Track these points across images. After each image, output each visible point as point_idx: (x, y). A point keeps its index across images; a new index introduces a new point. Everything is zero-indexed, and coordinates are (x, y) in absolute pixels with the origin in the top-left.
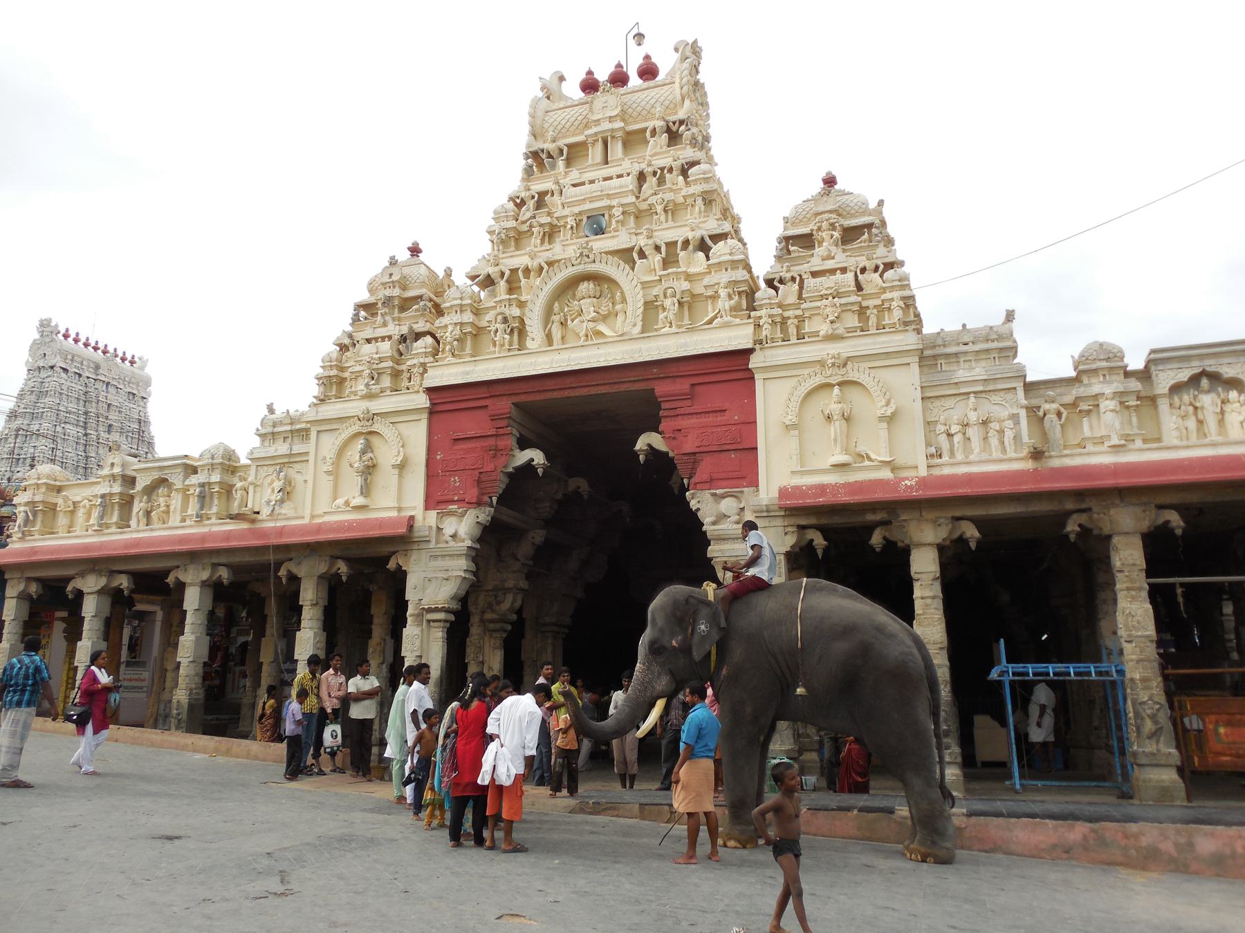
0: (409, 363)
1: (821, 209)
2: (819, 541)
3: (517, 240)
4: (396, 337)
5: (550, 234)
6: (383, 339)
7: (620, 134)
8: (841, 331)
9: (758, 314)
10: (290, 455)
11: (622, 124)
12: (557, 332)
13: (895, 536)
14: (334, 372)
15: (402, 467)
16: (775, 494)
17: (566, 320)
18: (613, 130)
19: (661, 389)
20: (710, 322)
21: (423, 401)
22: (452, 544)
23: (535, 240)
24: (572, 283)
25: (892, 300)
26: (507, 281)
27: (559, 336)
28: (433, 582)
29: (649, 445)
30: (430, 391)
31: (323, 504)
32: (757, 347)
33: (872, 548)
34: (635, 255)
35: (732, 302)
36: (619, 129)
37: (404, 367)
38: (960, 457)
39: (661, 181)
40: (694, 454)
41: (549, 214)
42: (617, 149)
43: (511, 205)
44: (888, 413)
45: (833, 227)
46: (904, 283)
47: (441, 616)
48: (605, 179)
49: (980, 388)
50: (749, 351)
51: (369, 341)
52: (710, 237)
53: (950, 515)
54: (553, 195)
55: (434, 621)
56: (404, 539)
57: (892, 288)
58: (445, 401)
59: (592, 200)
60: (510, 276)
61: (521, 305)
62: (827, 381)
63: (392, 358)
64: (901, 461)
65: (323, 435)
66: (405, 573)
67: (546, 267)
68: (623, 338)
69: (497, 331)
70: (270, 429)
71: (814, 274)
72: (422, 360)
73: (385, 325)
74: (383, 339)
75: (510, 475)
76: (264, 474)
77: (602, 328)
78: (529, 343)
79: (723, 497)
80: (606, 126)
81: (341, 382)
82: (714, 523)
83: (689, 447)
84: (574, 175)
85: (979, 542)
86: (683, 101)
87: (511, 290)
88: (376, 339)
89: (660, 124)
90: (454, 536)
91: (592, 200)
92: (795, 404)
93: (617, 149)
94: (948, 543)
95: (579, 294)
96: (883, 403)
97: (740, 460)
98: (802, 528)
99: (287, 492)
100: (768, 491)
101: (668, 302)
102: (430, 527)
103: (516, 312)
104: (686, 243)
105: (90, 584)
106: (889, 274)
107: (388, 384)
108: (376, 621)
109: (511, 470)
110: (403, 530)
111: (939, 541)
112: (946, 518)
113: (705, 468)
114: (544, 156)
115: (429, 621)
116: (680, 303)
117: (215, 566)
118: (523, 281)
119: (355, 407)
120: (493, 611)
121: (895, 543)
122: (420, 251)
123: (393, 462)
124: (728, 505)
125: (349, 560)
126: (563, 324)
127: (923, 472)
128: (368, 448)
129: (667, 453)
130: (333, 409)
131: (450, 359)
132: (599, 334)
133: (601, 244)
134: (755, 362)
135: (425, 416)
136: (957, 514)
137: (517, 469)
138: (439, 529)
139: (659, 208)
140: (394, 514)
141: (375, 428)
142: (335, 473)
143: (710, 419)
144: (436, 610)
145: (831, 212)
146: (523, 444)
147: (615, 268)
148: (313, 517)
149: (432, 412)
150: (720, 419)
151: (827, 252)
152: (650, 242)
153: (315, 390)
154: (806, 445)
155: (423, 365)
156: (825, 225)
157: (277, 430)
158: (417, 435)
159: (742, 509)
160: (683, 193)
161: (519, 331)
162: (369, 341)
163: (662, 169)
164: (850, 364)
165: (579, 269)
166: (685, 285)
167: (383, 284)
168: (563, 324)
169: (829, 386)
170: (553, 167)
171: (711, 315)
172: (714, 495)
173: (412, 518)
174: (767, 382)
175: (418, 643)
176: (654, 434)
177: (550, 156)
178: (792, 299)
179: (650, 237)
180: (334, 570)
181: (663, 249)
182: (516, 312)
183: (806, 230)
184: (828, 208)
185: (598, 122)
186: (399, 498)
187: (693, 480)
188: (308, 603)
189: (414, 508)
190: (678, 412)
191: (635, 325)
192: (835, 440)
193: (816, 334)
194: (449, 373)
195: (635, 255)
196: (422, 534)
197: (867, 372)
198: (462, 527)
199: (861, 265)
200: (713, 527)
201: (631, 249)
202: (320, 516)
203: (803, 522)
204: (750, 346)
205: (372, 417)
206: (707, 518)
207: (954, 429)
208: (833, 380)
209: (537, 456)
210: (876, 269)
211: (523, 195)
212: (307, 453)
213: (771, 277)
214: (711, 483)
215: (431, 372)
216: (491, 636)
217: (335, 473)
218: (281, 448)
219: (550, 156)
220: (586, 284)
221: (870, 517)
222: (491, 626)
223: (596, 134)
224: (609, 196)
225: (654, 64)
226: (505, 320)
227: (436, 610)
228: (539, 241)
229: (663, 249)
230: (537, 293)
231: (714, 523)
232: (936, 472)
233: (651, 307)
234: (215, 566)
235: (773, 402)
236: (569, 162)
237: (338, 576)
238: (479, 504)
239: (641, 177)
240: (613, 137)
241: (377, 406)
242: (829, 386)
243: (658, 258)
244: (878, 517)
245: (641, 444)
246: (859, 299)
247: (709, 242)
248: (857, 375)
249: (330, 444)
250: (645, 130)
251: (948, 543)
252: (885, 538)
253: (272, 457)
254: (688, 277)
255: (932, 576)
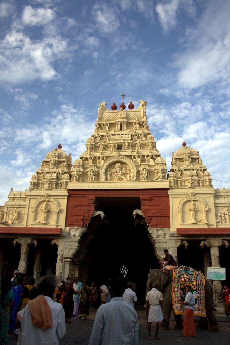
0: (62, 181)
1: (185, 152)
2: (186, 244)
3: (94, 148)
4: (57, 173)
5: (105, 148)
6: (52, 172)
7: (126, 122)
8: (193, 186)
9: (170, 179)
10: (20, 205)
11: (126, 120)
12: (109, 178)
13: (207, 243)
14: (36, 181)
15: (59, 212)
16: (175, 230)
17: (112, 174)
18: (124, 121)
19: (142, 197)
20: (157, 179)
21: (66, 193)
22: (73, 238)
23: (100, 149)
24: (115, 163)
25: (207, 179)
26: (93, 160)
27: (109, 178)
28: (66, 249)
29: (137, 213)
30: (68, 190)
31: (32, 221)
32: (171, 188)
33: (200, 247)
34: (132, 158)
35: (163, 175)
36: (125, 121)
37: (60, 182)
38: (224, 222)
39: (138, 137)
40: (151, 217)
41: (104, 142)
42: (125, 126)
43: (93, 138)
44: (207, 210)
45: (189, 157)
46: (209, 175)
47: (69, 260)
48: (122, 135)
49: (18, 206)
50: (168, 189)
51: (48, 173)
52: (155, 155)
53: (222, 239)
54: (105, 136)
55: (67, 261)
56: (59, 235)
57: (206, 176)
58: (73, 194)
59: (118, 140)
60: (93, 159)
61: (97, 167)
62: (190, 199)
63: (56, 179)
64: (210, 223)
65: (31, 200)
66: (57, 246)
67: (105, 158)
68: (131, 181)
69: (90, 175)
70: (13, 196)
71: (185, 170)
72: (66, 181)
73: (53, 168)
74: (52, 172)
75: (92, 218)
76: (9, 210)
77: (123, 177)
78: (101, 180)
79: (160, 230)
80: (121, 120)
81: (38, 184)
82: (157, 238)
83: (149, 215)
84: (112, 132)
85: (229, 246)
86: (144, 116)
87: (93, 163)
88: (50, 172)
89: (137, 122)
90: (74, 236)
91: (118, 140)
92: (181, 205)
93: (125, 126)
94: (221, 246)
95: (116, 167)
96: (205, 207)
97: (164, 220)
98: (182, 240)
99: (19, 216)
100: (173, 229)
101: (144, 172)
102: (67, 232)
103: (97, 170)
104: (148, 156)
105: (24, 243)
106: (205, 172)
107: (55, 187)
108: (37, 259)
109: (93, 217)
110: (59, 233)
111: (219, 246)
112: (221, 239)
113: (154, 221)
114: (102, 125)
115: (65, 261)
116: (147, 173)
117: (33, 239)
118: (98, 161)
119: (44, 193)
120: (77, 259)
121: (56, 244)
122: (61, 147)
123: (56, 211)
124: (160, 232)
125: (38, 241)
126: (111, 175)
127: (215, 227)
128: (47, 205)
129: (143, 216)
130: (35, 192)
131: (81, 182)
132: (122, 179)
133: (123, 153)
134: (170, 192)
135: (66, 198)
136: (33, 238)
137: (95, 217)
138: (69, 233)
139: (139, 145)
140: (55, 227)
141: (50, 200)
142: (36, 212)
143: (156, 207)
144: (68, 258)
145: (188, 153)
146: (97, 210)
147: (128, 161)
148: (27, 225)
149: (69, 197)
150: (159, 207)
151: (186, 164)
152: (137, 154)
153: (29, 186)
154: (184, 216)
155: (66, 182)
156: (187, 157)
157: (15, 196)
158: (64, 203)
159: (165, 234)
160: (108, 143)
161: (97, 175)
162: (48, 173)
163: (139, 134)
164: (196, 196)
165: (117, 159)
166: (149, 168)
167: (52, 156)
168: (111, 175)
169: (45, 201)
170: (105, 128)
171: (156, 178)
172: (157, 229)
173: (61, 229)
174: (173, 198)
175: (61, 268)
176: (139, 210)
177: (104, 125)
178: (179, 175)
179: (137, 153)
180: (32, 243)
181: (141, 157)
182: (97, 170)
183: (182, 157)
184: (187, 152)
185: (119, 118)
186: (57, 222)
187: (150, 224)
188: (24, 253)
189: (62, 226)
190: (146, 204)
191: (134, 178)
192: (192, 216)
193: (186, 186)
194: (75, 185)
195: (132, 158)
196: (64, 234)
197: (200, 198)
198: (76, 232)
199: (197, 169)
200: (157, 239)
201: (132, 156)
202: (29, 225)
203: (183, 238)
204: (169, 188)
205: (48, 196)
206: (154, 236)
207: (223, 215)
208: (191, 199)
209: (102, 213)
210: (201, 170)
211: (96, 135)
212: (26, 205)
213: (38, 172)
214: (156, 226)
215: (69, 185)
216: (75, 266)
217: (36, 212)
218: (17, 202)
219: (104, 125)
220: (118, 164)
221: (201, 238)
222: (76, 263)
223: (119, 121)
224: (124, 140)
225: (133, 105)
226: (93, 172)
227: (68, 258)
228: (102, 150)
229: (141, 157)
230: (103, 165)
231: (157, 238)
232: (219, 227)
233: (138, 173)
234: (33, 239)
235: (175, 204)
236: (109, 128)
237: (33, 244)
238: (83, 226)
239: (132, 136)
240: (123, 123)
241: (196, 191)
242: (190, 201)
243: (139, 159)
244: (203, 239)
245: (135, 212)
246: (198, 178)
247: (155, 157)
248: (198, 199)
249: (34, 203)
250: (133, 122)
251: (221, 246)
252: (204, 244)
253: (13, 205)
254: (149, 166)
255: (217, 255)
